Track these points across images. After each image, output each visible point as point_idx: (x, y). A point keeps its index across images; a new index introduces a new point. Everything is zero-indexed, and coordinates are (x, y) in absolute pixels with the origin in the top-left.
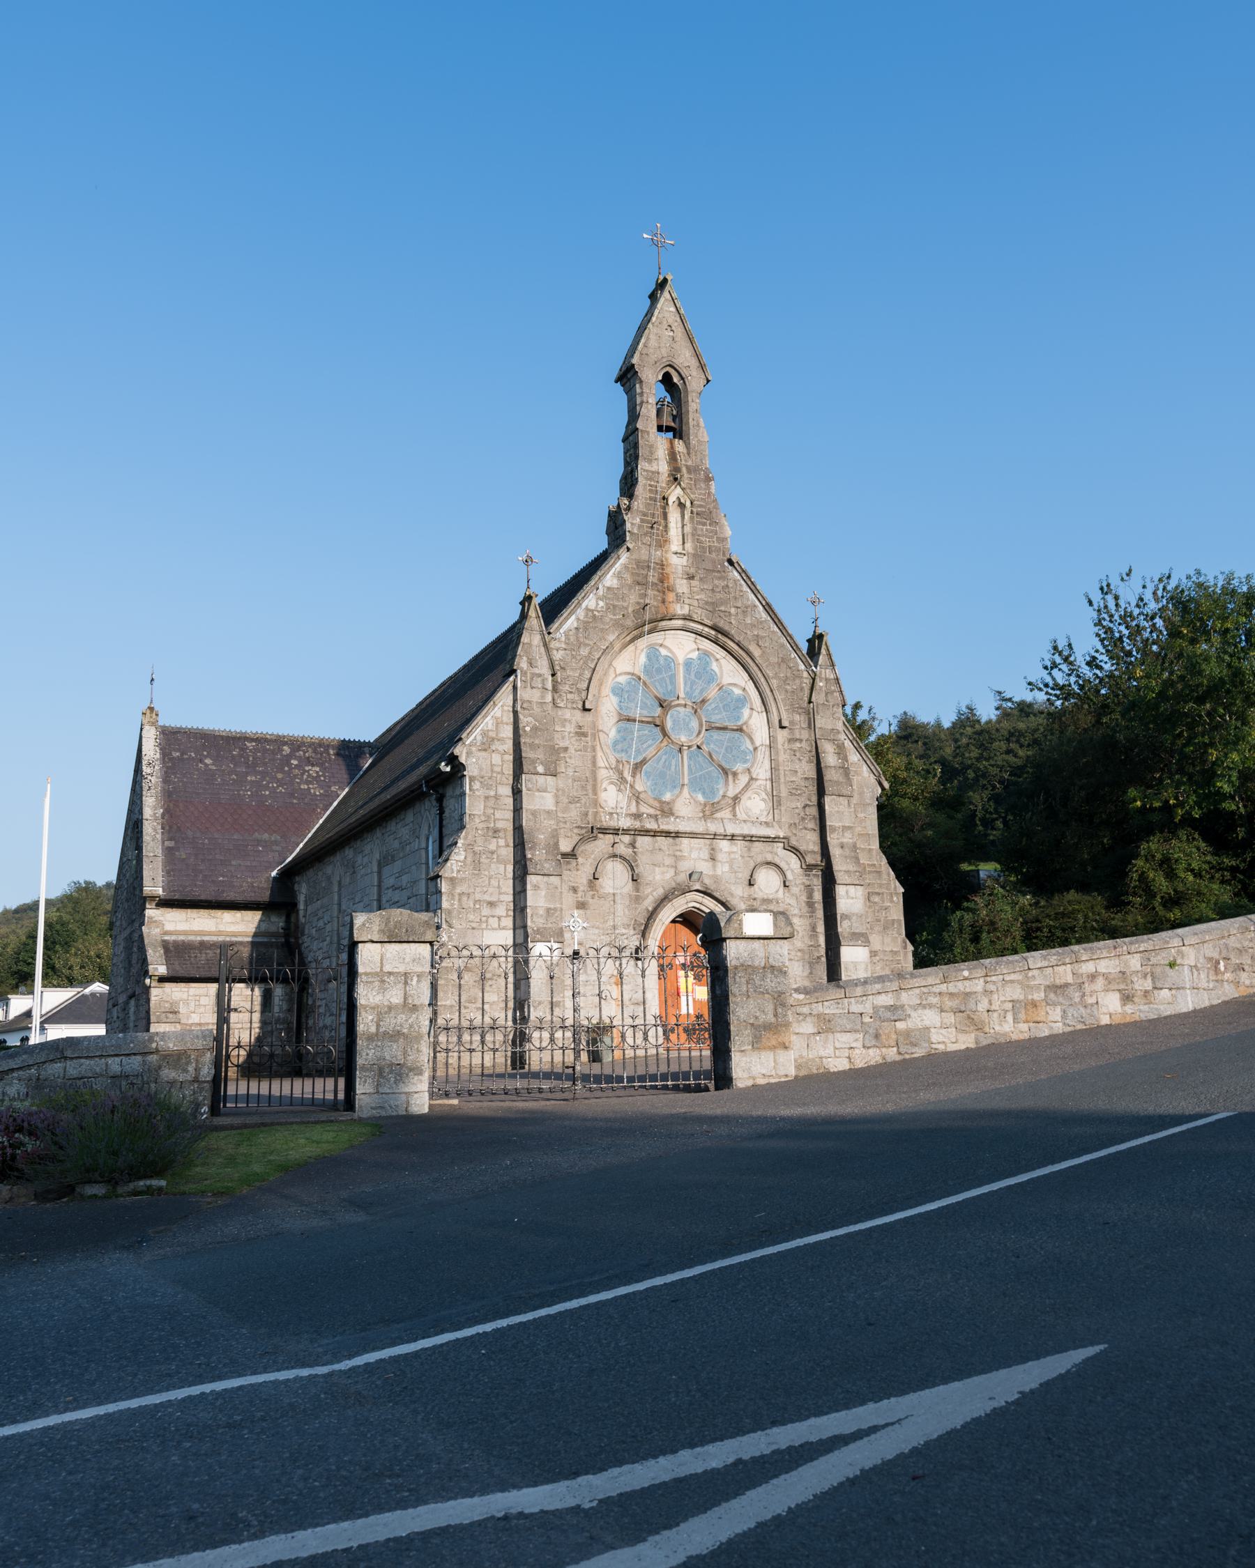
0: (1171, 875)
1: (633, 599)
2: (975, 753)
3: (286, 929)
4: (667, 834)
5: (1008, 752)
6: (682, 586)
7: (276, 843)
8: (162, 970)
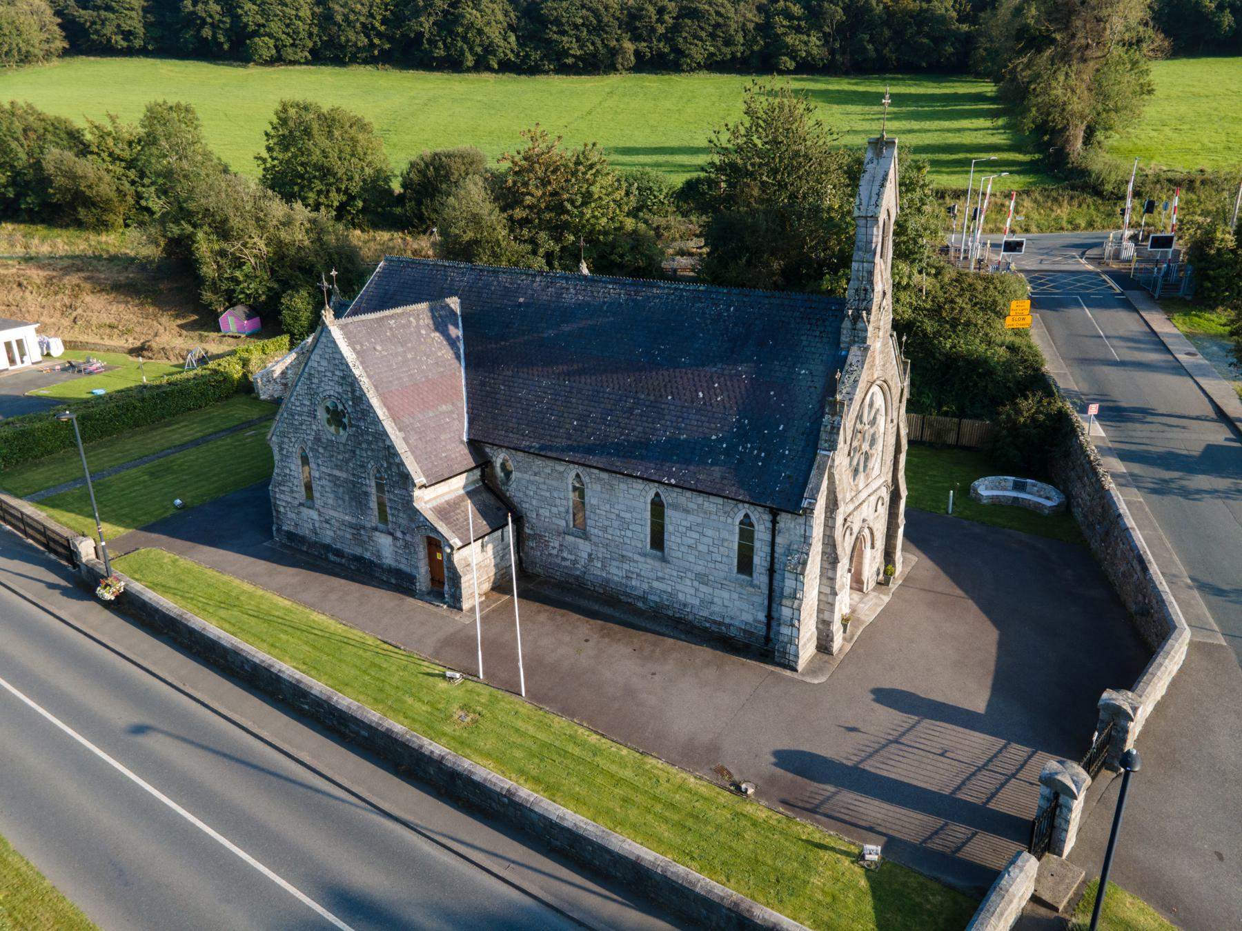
7: (452, 412)
8: (460, 544)
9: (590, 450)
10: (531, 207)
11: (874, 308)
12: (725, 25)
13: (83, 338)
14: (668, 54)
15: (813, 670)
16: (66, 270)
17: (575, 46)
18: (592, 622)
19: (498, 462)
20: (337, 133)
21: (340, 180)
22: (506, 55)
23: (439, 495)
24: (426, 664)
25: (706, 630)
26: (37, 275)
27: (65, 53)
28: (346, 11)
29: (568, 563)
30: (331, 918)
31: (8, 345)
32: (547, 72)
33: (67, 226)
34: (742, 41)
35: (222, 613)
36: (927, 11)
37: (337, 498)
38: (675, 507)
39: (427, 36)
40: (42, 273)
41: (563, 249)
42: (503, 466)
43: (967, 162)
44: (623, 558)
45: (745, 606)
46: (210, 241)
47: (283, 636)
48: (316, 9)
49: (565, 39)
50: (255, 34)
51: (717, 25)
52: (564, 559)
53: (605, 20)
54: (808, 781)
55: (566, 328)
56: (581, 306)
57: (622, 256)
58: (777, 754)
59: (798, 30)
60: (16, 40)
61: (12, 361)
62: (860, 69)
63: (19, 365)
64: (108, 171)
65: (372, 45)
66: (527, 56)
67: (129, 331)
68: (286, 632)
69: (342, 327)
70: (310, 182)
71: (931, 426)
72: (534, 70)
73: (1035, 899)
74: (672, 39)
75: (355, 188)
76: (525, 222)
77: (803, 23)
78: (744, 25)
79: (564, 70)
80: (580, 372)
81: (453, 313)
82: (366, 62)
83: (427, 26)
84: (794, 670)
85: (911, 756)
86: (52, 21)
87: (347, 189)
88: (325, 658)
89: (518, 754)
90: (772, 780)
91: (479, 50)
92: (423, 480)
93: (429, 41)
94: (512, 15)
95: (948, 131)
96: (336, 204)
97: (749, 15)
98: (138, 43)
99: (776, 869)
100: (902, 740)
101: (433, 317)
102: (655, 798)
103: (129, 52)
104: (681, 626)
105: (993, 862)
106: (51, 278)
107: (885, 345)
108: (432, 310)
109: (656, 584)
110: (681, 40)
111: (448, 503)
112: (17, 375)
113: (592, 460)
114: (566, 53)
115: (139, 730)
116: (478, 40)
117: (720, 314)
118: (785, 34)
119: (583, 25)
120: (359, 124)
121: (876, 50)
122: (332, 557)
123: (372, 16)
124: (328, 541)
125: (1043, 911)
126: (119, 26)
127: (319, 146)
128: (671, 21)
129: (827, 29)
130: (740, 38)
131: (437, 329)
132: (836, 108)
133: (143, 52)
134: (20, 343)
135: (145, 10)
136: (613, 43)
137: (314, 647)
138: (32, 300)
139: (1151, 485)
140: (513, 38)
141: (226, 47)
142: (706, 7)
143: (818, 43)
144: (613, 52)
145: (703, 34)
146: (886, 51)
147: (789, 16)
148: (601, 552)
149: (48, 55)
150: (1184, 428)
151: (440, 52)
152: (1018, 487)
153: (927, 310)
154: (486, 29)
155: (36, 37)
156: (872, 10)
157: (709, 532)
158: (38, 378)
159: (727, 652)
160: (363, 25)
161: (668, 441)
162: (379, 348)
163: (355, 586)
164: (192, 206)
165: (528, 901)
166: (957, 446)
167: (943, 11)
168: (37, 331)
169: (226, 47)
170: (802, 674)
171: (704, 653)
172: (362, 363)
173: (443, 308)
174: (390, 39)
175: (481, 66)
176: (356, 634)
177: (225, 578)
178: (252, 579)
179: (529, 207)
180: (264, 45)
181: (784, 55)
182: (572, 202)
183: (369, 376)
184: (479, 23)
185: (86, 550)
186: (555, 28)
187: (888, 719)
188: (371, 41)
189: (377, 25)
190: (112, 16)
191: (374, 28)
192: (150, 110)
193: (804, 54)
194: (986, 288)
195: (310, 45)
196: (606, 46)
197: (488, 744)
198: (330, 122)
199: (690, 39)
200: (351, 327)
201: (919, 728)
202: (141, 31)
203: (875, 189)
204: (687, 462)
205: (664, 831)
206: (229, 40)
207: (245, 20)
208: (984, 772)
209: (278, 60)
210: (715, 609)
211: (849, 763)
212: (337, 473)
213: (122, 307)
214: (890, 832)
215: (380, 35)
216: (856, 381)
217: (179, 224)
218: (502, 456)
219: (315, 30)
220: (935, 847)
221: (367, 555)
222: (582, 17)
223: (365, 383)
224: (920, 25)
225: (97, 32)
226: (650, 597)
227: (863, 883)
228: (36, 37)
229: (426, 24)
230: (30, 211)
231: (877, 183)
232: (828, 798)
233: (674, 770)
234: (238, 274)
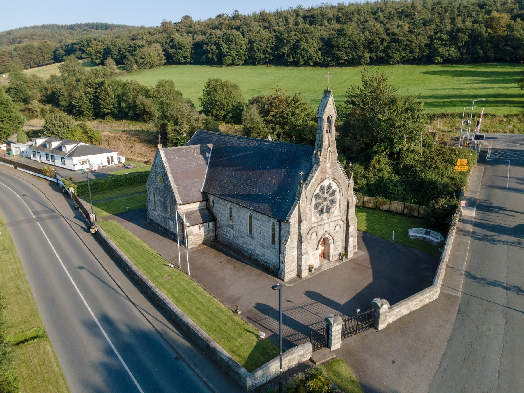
0: (379, 164)
1: (320, 177)
2: (286, 34)
3: (206, 204)
4: (323, 225)
5: (296, 35)
6: (328, 170)
7: (199, 181)
8: (188, 225)
9: (233, 196)
10: (273, 116)
11: (323, 151)
12: (411, 45)
13: (133, 157)
14: (384, 58)
16: (133, 135)
17: (344, 55)
18: (227, 257)
19: (211, 200)
20: (225, 90)
21: (224, 106)
22: (316, 60)
23: (187, 208)
25: (263, 265)
26: (124, 136)
27: (165, 64)
28: (258, 46)
29: (228, 238)
30: (98, 323)
31: (108, 158)
32: (333, 66)
33: (140, 121)
34: (418, 51)
35: (119, 240)
36: (510, 35)
37: (161, 208)
38: (255, 218)
39: (286, 53)
40: (126, 136)
41: (284, 132)
42: (213, 201)
43: (471, 103)
44: (242, 236)
45: (274, 257)
46: (172, 126)
47: (131, 249)
48: (248, 46)
49: (340, 53)
50: (226, 55)
51: (408, 45)
52: (227, 236)
53: (358, 45)
55: (238, 155)
56: (244, 147)
57: (305, 135)
59: (445, 45)
60: (149, 60)
61: (109, 163)
62: (476, 61)
63: (111, 165)
64: (154, 103)
65: (266, 58)
66: (325, 60)
67: (146, 156)
68: (132, 247)
69: (164, 151)
70: (214, 106)
71: (407, 208)
72: (327, 65)
74: (387, 51)
75: (230, 109)
76: (270, 122)
77: (448, 43)
78: (420, 44)
79: (339, 65)
81: (209, 149)
82: (263, 64)
83: (286, 50)
84: (283, 281)
85: (304, 313)
86: (162, 53)
87: (227, 109)
88: (139, 256)
89: (175, 290)
91: (306, 58)
92: (181, 202)
93: (287, 56)
94: (320, 45)
95: (503, 88)
96: (223, 115)
97: (423, 40)
98: (188, 60)
100: (305, 308)
101: (201, 149)
102: (208, 309)
103: (185, 63)
104: (256, 263)
106: (128, 137)
107: (333, 165)
108: (201, 147)
109: (251, 247)
110: (390, 52)
111: (190, 212)
112: (111, 167)
113: (233, 200)
114: (340, 58)
115: (81, 268)
116: (306, 55)
117: (282, 152)
118: (439, 47)
119: (349, 47)
120: (235, 87)
121: (484, 52)
122: (159, 228)
123: (267, 47)
124: (159, 222)
126: (182, 54)
127: (220, 95)
128: (386, 44)
129: (460, 45)
130: (417, 50)
131: (201, 154)
132: (456, 78)
133: (190, 63)
134: (112, 157)
135: (192, 49)
136: (360, 54)
137: (138, 253)
138: (122, 144)
139: (479, 237)
140: (320, 53)
141: (216, 60)
142: (403, 38)
143: (455, 50)
144: (360, 57)
145: (400, 49)
146: (489, 53)
147: (441, 39)
148: (237, 234)
149: (159, 65)
150: (515, 216)
151: (291, 59)
152: (427, 233)
153: (422, 161)
154: (309, 50)
155: (156, 59)
156: (483, 36)
157: (264, 228)
158: (112, 169)
159: (265, 272)
160: (264, 50)
161: (256, 194)
162: (177, 158)
163: (161, 237)
164: (167, 114)
165: (153, 328)
166: (418, 217)
167: (519, 36)
168: (118, 154)
169: (216, 60)
172: (168, 162)
173: (205, 147)
174: (273, 55)
175: (306, 64)
176: (152, 251)
177: (126, 230)
178: (133, 232)
179: (272, 116)
180: (228, 60)
181: (438, 56)
182: (287, 114)
183: (170, 167)
184: (306, 48)
185: (92, 216)
186: (336, 49)
187: (308, 300)
188: (266, 56)
189: (269, 50)
190: (181, 51)
191: (267, 51)
192: (159, 82)
193: (447, 56)
194: (450, 154)
195: (244, 58)
196: (357, 55)
198: (224, 85)
199: (394, 51)
200: (168, 151)
201: (314, 305)
202: (189, 56)
205: (203, 318)
206: (217, 57)
207: (223, 51)
209: (232, 64)
210: (266, 257)
212: (161, 199)
213: (145, 147)
215: (269, 54)
217: (164, 120)
218: (212, 198)
219: (246, 53)
221: (167, 228)
222: (348, 44)
223: (168, 169)
224: (507, 41)
225: (175, 57)
226: (249, 252)
228: (156, 59)
229: (286, 49)
230: (131, 116)
232: (264, 319)
234: (179, 137)
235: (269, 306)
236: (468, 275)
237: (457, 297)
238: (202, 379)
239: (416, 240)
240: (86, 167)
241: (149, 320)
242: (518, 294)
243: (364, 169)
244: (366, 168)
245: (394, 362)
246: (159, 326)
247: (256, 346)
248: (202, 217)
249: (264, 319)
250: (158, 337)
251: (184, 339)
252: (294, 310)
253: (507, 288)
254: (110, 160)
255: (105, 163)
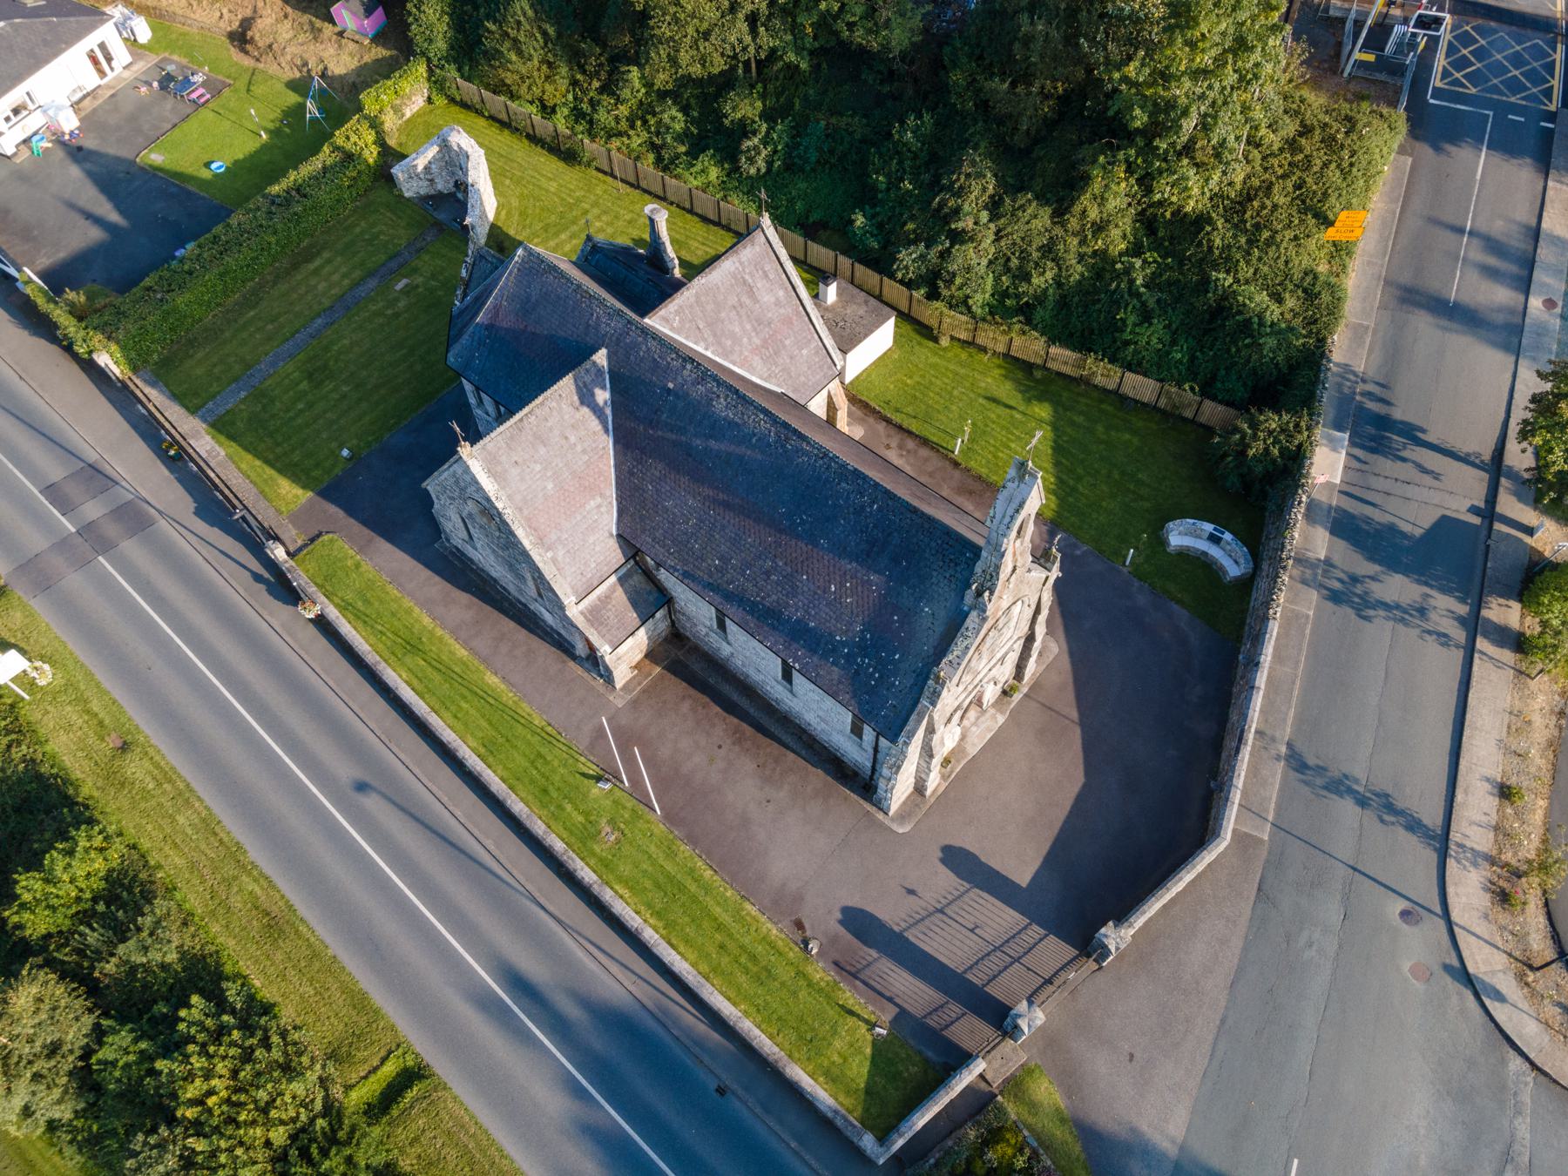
15: (902, 816)
24: (582, 759)
54: (860, 944)
56: (731, 424)
58: (846, 910)
61: (102, 73)
63: (110, 75)
73: (981, 1076)
80: (727, 506)
81: (600, 371)
90: (834, 940)
99: (813, 1029)
105: (967, 1044)
115: (361, 787)
117: (863, 507)
125: (983, 1085)
131: (582, 403)
134: (102, 46)
150: (1436, 476)
170: (892, 819)
171: (818, 777)
187: (946, 880)
197: (625, 869)
203: (1010, 512)
204: (813, 651)
208: (998, 953)
211: (896, 929)
214: (906, 1006)
216: (967, 648)
220: (931, 1023)
227: (868, 1051)
231: (1014, 506)
233: (763, 919)
235: (872, 916)
236: (1297, 762)
237: (1261, 841)
238: (788, 1145)
239: (1184, 555)
240: (33, 122)
241: (618, 981)
242: (1382, 821)
243: (1052, 217)
244: (1060, 214)
245: (1132, 1056)
246: (641, 991)
247: (873, 1056)
248: (635, 604)
249: (869, 965)
250: (651, 1023)
251: (716, 1030)
252: (927, 922)
253: (1362, 802)
254: (100, 59)
255: (91, 80)
